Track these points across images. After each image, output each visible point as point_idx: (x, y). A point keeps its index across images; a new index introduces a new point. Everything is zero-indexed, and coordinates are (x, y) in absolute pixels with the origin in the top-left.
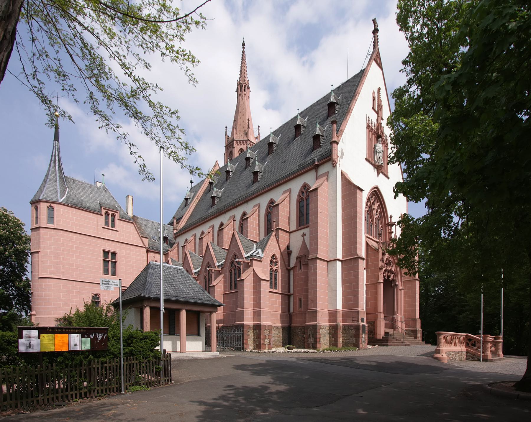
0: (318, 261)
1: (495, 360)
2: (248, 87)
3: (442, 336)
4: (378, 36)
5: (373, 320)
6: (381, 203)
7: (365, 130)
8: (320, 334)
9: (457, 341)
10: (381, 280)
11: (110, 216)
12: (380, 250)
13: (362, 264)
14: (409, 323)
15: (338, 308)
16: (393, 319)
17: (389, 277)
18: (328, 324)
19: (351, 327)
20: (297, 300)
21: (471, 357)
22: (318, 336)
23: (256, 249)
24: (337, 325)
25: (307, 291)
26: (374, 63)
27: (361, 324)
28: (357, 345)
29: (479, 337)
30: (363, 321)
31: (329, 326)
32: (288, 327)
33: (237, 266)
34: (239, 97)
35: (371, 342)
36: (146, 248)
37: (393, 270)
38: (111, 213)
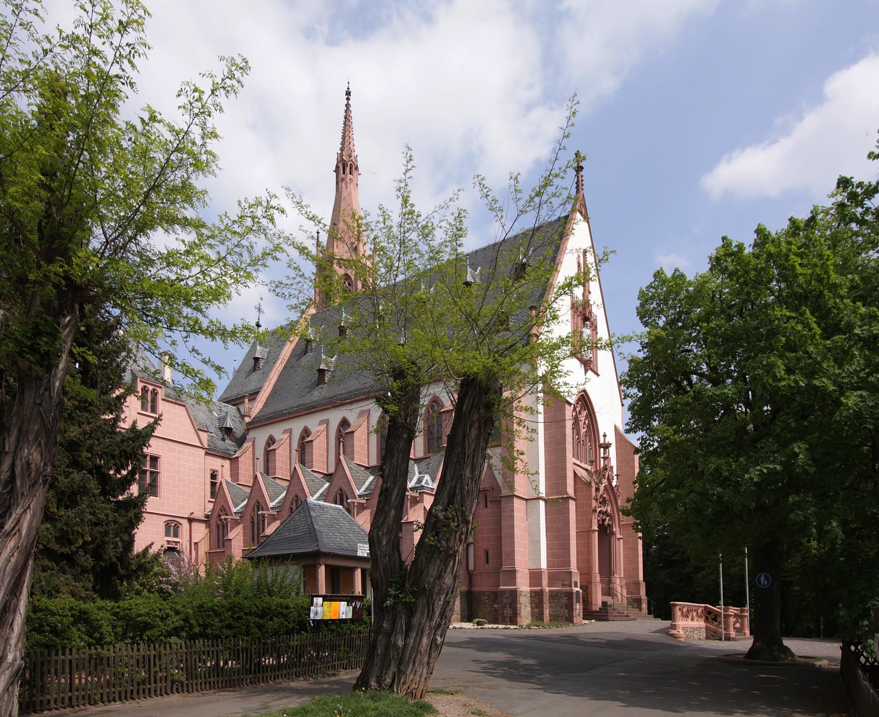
0: (515, 499)
1: (739, 639)
2: (357, 168)
3: (678, 608)
4: (582, 176)
5: (586, 584)
6: (589, 411)
8: (520, 604)
9: (695, 614)
10: (595, 527)
11: (149, 393)
12: (593, 485)
13: (572, 505)
14: (632, 586)
15: (542, 567)
16: (610, 582)
17: (604, 521)
18: (528, 589)
20: (482, 553)
21: (712, 635)
22: (518, 606)
24: (542, 590)
25: (499, 539)
27: (575, 589)
28: (570, 619)
29: (720, 609)
30: (576, 586)
31: (531, 591)
32: (468, 592)
34: (340, 183)
35: (587, 615)
36: (204, 449)
37: (609, 511)
38: (151, 388)
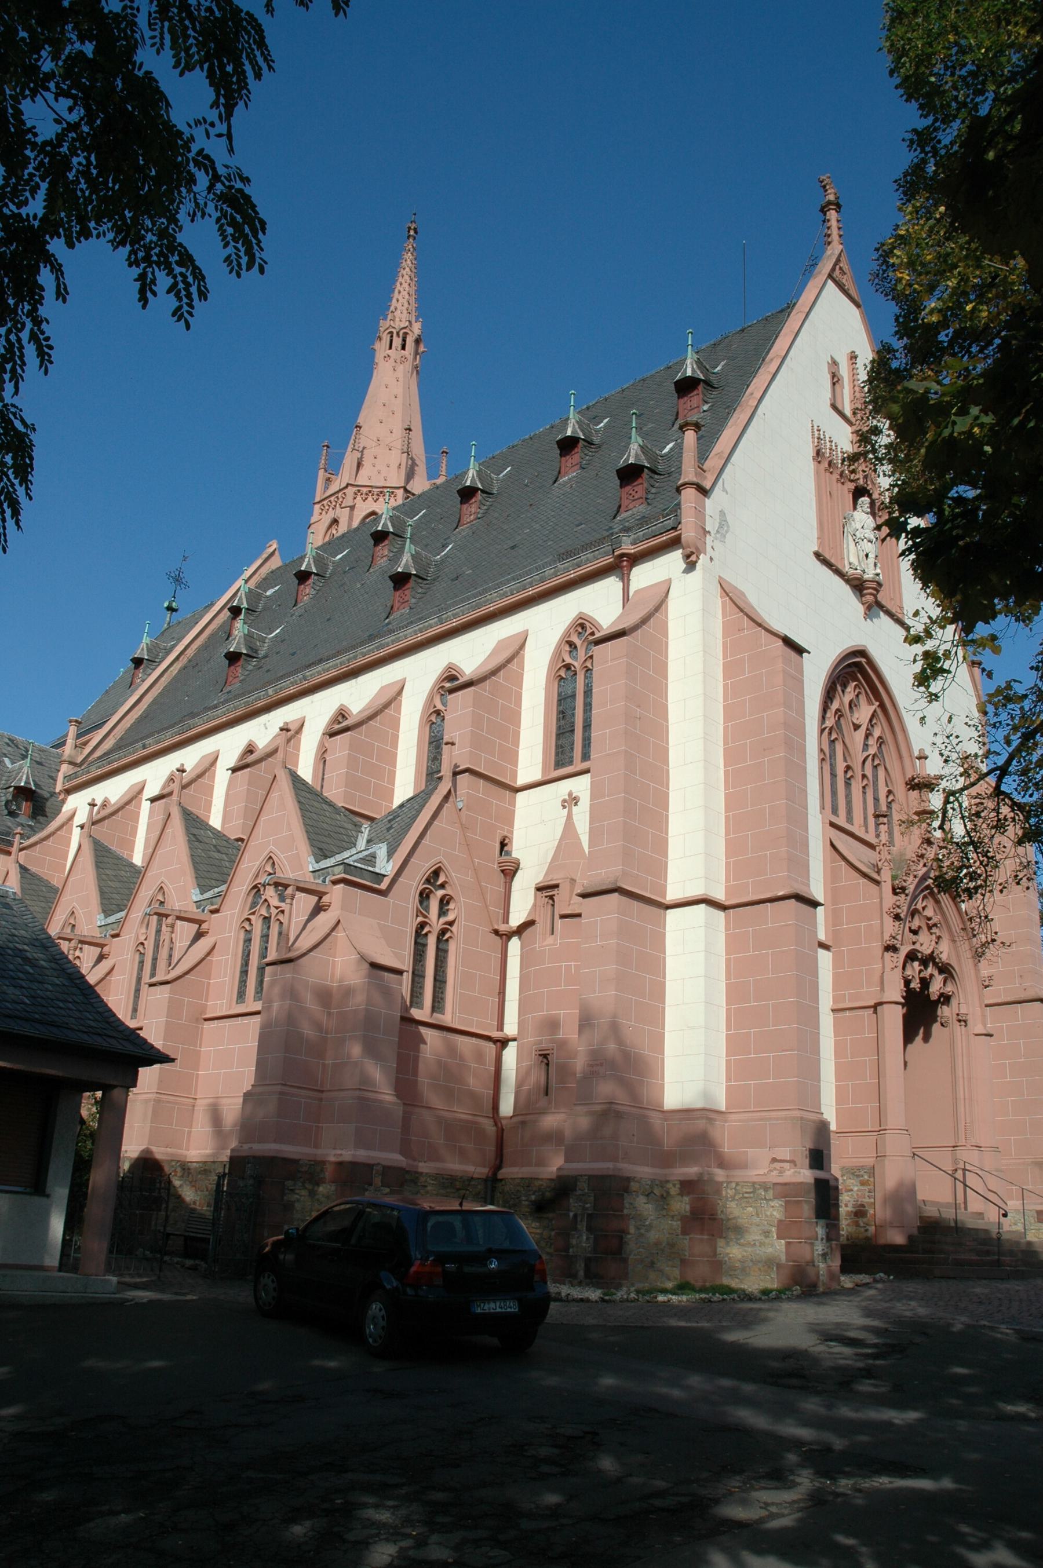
7: (809, 466)
17: (925, 983)
19: (766, 1189)
23: (369, 841)
26: (829, 281)
32: (486, 1180)
33: (277, 908)
